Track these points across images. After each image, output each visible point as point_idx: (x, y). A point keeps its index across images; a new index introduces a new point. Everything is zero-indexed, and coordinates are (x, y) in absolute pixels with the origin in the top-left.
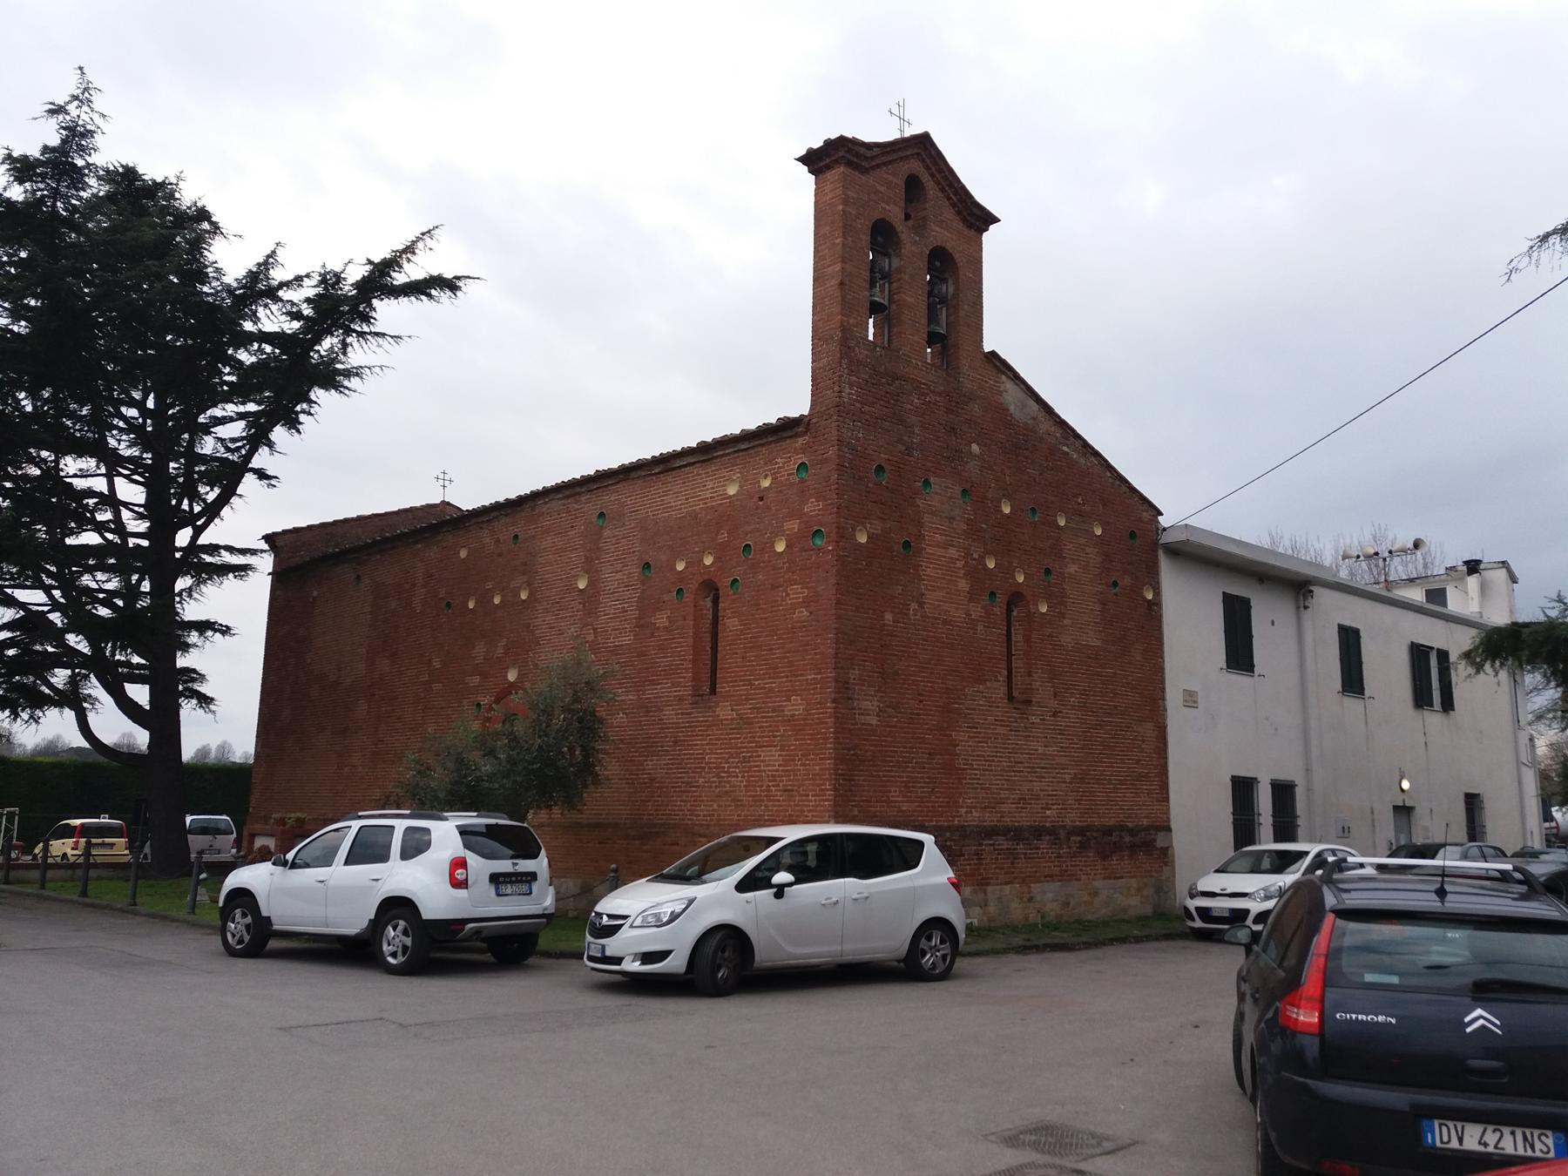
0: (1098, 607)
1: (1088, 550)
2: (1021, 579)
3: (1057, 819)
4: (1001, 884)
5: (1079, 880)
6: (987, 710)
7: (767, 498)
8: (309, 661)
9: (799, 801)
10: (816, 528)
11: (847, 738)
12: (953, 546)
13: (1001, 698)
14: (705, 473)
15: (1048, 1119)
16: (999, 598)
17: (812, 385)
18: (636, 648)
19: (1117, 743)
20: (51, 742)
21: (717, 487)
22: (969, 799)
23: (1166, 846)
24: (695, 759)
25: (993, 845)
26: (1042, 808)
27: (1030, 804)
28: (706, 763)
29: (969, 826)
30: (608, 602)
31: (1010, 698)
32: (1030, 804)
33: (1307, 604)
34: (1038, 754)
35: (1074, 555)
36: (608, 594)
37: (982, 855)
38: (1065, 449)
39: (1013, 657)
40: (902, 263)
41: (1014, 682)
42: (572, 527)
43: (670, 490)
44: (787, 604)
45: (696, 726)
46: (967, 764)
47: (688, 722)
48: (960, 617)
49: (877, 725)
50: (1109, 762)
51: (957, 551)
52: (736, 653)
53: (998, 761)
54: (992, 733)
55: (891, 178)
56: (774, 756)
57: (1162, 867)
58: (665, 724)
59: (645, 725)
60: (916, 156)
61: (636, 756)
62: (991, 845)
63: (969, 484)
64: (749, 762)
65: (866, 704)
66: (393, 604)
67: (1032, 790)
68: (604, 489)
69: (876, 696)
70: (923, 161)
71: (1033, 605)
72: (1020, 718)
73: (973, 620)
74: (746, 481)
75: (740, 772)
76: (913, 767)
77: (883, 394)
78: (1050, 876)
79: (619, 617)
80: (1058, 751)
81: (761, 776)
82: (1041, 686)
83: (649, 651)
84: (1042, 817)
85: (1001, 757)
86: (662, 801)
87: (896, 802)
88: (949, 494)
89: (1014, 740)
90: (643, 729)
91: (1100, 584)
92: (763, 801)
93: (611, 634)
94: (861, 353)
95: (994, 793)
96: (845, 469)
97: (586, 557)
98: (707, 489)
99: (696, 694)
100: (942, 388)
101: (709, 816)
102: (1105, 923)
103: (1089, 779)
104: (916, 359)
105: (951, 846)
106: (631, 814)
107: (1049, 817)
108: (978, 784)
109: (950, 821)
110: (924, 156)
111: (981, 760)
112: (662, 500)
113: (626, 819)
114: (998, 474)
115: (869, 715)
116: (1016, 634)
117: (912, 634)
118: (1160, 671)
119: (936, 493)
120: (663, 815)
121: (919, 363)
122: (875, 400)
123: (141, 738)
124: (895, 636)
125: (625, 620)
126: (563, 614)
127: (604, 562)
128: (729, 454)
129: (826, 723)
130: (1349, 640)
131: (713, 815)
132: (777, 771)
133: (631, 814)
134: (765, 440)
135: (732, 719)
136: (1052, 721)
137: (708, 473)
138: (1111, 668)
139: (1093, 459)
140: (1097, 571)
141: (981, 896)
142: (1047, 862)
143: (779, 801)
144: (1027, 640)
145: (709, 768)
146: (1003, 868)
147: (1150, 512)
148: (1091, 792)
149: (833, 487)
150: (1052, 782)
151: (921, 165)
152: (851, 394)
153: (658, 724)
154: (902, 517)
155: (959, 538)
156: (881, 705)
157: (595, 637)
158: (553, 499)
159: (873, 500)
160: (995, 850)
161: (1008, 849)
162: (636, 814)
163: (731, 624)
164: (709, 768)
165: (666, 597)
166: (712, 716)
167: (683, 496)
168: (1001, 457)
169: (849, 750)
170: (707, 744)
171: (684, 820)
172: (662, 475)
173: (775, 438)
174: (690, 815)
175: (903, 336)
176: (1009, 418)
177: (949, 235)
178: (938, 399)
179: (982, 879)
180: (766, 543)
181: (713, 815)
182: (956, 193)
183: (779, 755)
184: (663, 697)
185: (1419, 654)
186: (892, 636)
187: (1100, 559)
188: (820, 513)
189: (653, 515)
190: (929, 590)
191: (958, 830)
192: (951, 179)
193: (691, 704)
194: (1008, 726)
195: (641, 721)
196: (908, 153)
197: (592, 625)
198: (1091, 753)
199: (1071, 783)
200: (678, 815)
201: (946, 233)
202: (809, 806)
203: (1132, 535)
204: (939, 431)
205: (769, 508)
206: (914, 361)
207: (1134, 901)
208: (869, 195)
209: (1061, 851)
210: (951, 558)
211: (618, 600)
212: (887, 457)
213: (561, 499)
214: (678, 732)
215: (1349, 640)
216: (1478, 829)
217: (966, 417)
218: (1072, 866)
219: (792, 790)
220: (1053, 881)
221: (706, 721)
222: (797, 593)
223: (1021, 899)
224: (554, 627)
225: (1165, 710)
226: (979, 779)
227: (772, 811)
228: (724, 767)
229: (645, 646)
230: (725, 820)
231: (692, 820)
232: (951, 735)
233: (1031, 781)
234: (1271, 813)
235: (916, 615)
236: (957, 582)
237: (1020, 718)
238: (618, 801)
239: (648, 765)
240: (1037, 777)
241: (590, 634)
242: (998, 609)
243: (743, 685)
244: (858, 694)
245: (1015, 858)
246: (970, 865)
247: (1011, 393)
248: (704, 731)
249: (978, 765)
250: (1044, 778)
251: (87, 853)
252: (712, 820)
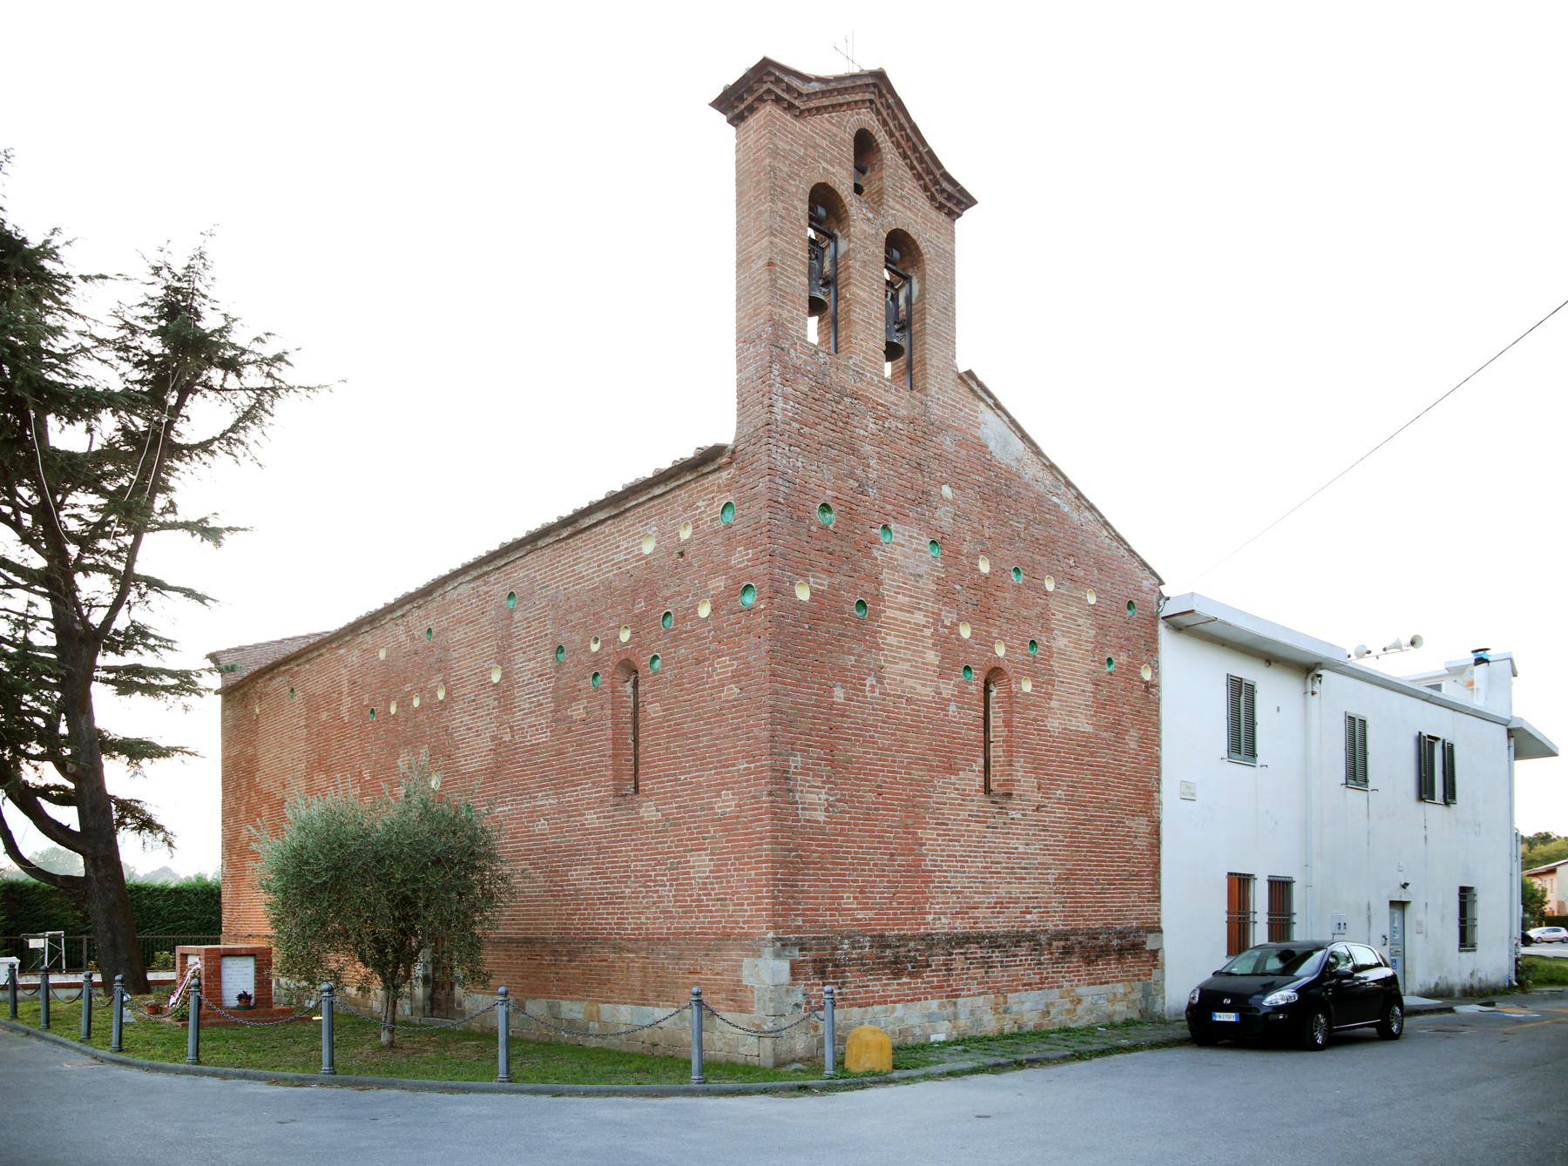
0: (1090, 687)
1: (1080, 621)
2: (1000, 651)
3: (1038, 924)
4: (974, 995)
5: (1061, 987)
6: (960, 805)
7: (689, 553)
8: (258, 780)
9: (734, 911)
10: (745, 583)
11: (788, 837)
12: (919, 609)
13: (976, 791)
14: (618, 531)
15: (929, 339)
16: (976, 674)
17: (738, 403)
18: (553, 746)
19: (1107, 839)
21: (632, 546)
22: (938, 903)
23: (1155, 948)
24: (620, 867)
25: (965, 953)
26: (1021, 912)
27: (1008, 908)
28: (632, 871)
29: (937, 934)
30: (522, 696)
31: (987, 789)
32: (1008, 908)
33: (1315, 690)
34: (1019, 853)
35: (1063, 626)
36: (523, 686)
37: (951, 965)
38: (1055, 499)
39: (992, 745)
40: (852, 245)
41: (992, 773)
42: (483, 613)
43: (581, 557)
44: (714, 682)
45: (619, 831)
46: (935, 866)
47: (611, 826)
48: (928, 696)
49: (825, 822)
50: (1098, 861)
51: (925, 616)
52: (659, 744)
53: (972, 862)
54: (966, 831)
55: (835, 130)
56: (703, 861)
57: (1150, 970)
58: (587, 829)
59: (567, 832)
60: (868, 104)
61: (559, 866)
62: (961, 954)
63: (940, 535)
64: (677, 869)
65: (811, 798)
66: (324, 716)
67: (1010, 893)
68: (512, 565)
69: (824, 788)
70: (878, 113)
71: (1017, 683)
72: (998, 813)
73: (944, 699)
74: (663, 534)
75: (668, 880)
76: (870, 870)
77: (829, 414)
78: (1030, 984)
79: (534, 712)
80: (1041, 849)
81: (691, 884)
82: (1023, 777)
83: (567, 748)
84: (1022, 922)
85: (976, 857)
86: (589, 914)
87: (849, 909)
88: (914, 546)
89: (991, 837)
90: (565, 837)
91: (1092, 661)
92: (694, 912)
93: (527, 732)
94: (797, 357)
95: (967, 897)
96: (779, 506)
97: (499, 647)
98: (621, 551)
99: (619, 794)
100: (905, 413)
101: (637, 929)
102: (1090, 1030)
103: (1074, 879)
104: (871, 373)
105: (915, 957)
106: (558, 929)
107: (1030, 922)
108: (947, 887)
109: (914, 929)
110: (879, 106)
111: (952, 861)
112: (573, 571)
113: (554, 934)
114: (975, 525)
115: (816, 810)
116: (994, 717)
117: (869, 714)
118: (1155, 760)
119: (898, 544)
120: (589, 928)
121: (876, 378)
122: (817, 421)
123: (73, 864)
124: (848, 717)
125: (541, 715)
126: (480, 712)
127: (516, 650)
128: (642, 504)
129: (762, 820)
130: (1356, 732)
131: (641, 929)
132: (708, 877)
133: (558, 929)
134: (682, 481)
135: (657, 821)
136: (1036, 816)
137: (621, 530)
138: (1103, 757)
139: (1087, 513)
140: (1090, 647)
141: (950, 1009)
142: (1025, 970)
143: (711, 911)
144: (1008, 724)
145: (636, 877)
146: (975, 979)
147: (1151, 581)
148: (1076, 893)
149: (764, 529)
150: (1034, 883)
151: (875, 118)
152: (785, 410)
153: (579, 830)
154: (855, 571)
155: (927, 600)
156: (831, 798)
157: (513, 736)
159: (817, 548)
160: (967, 959)
161: (981, 957)
162: (563, 929)
163: (653, 710)
164: (636, 877)
165: (582, 685)
166: (636, 819)
167: (595, 562)
168: (978, 504)
169: (790, 850)
170: (632, 850)
171: (611, 934)
172: (571, 540)
173: (695, 475)
174: (618, 929)
175: (854, 341)
176: (988, 457)
177: (912, 216)
178: (900, 426)
179: (952, 991)
180: (688, 609)
181: (641, 929)
182: (921, 160)
183: (711, 860)
184: (583, 799)
185: (1425, 745)
186: (842, 716)
187: (1092, 633)
188: (750, 564)
189: (565, 589)
190: (890, 662)
191: (923, 939)
192: (914, 139)
193: (612, 806)
194: (985, 822)
195: (563, 827)
196: (857, 98)
197: (508, 723)
198: (1078, 851)
199: (1054, 884)
200: (605, 929)
201: (909, 213)
202: (744, 916)
203: (1130, 605)
204: (901, 467)
205: (690, 565)
206: (868, 375)
207: (1120, 1007)
208: (806, 149)
209: (1042, 958)
210: (919, 625)
211: (533, 692)
212: (835, 494)
213: (469, 582)
214: (600, 838)
215: (1356, 732)
216: (1469, 922)
217: (937, 451)
218: (1053, 972)
219: (726, 899)
220: (1032, 989)
221: (630, 824)
222: (725, 666)
223: (996, 1009)
224: (471, 728)
225: (1160, 803)
226: (949, 882)
227: (704, 923)
228: (651, 876)
229: (562, 743)
230: (653, 934)
231: (621, 934)
232: (916, 833)
233: (1009, 883)
234: (1267, 910)
235: (874, 692)
236: (925, 653)
237: (998, 813)
239: (572, 875)
240: (1016, 878)
241: (506, 733)
242: (974, 687)
243: (668, 781)
244: (801, 785)
245: (991, 967)
246: (938, 976)
247: (990, 428)
248: (628, 835)
249: (949, 866)
250: (1024, 879)
252: (640, 934)
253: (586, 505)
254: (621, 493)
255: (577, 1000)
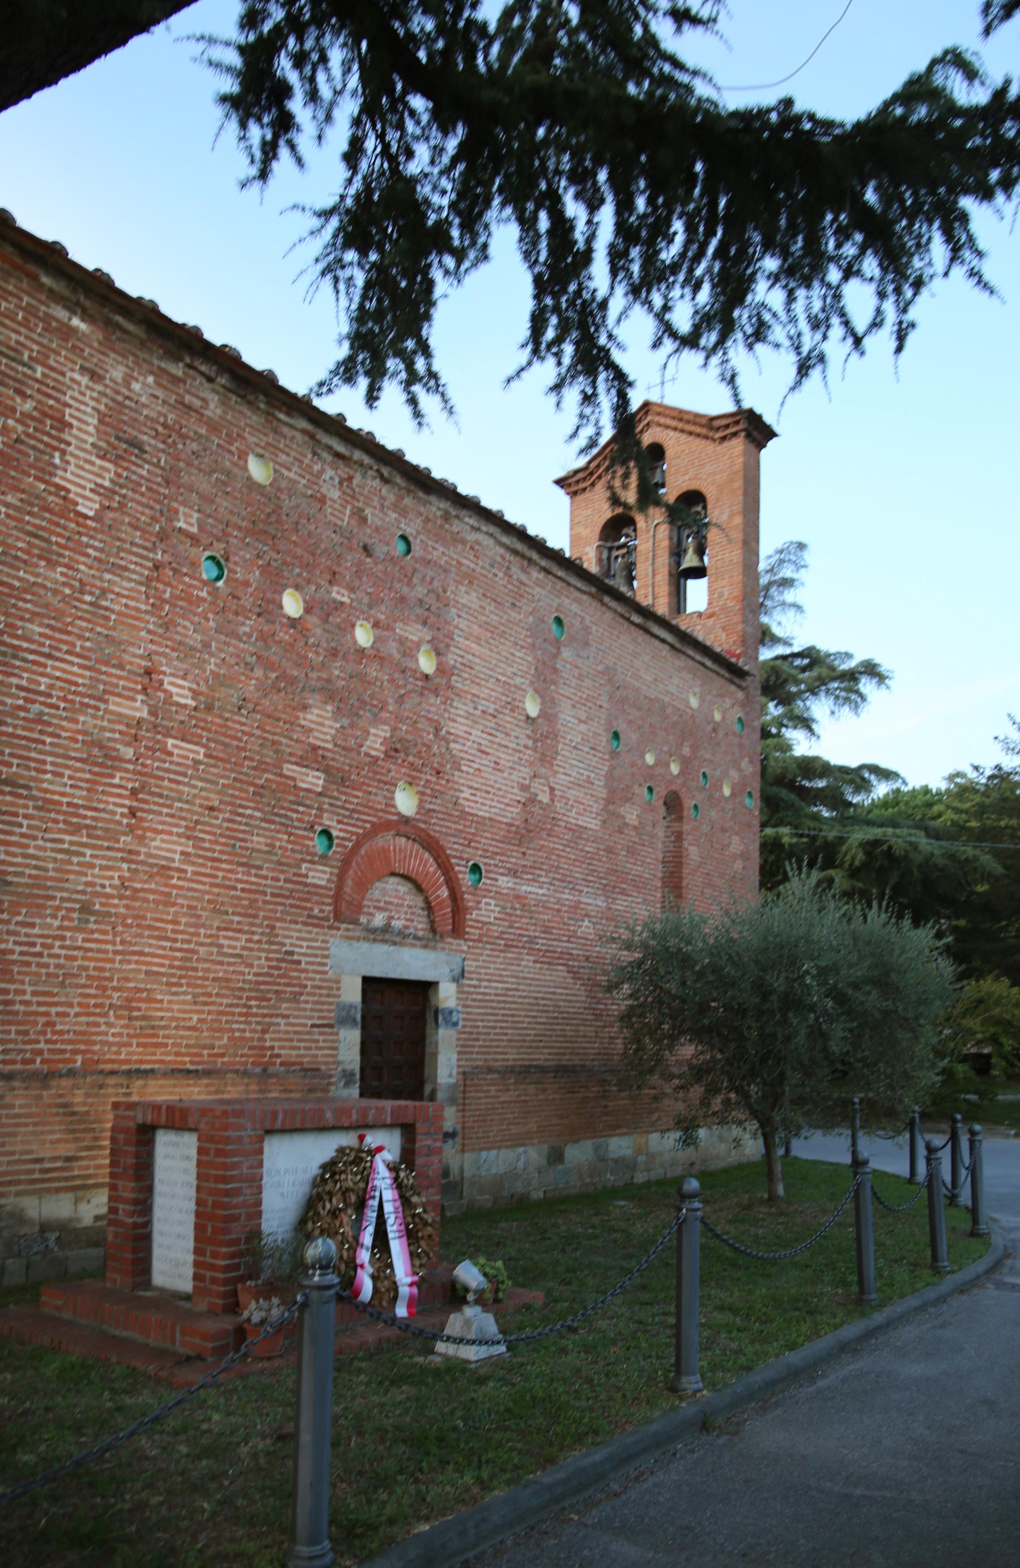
20: (662, 937)
158: (491, 535)
173: (727, 675)
213: (507, 548)
238: (585, 1037)
251: (362, 1138)
253: (391, 446)
254: (433, 480)
255: (625, 1134)
